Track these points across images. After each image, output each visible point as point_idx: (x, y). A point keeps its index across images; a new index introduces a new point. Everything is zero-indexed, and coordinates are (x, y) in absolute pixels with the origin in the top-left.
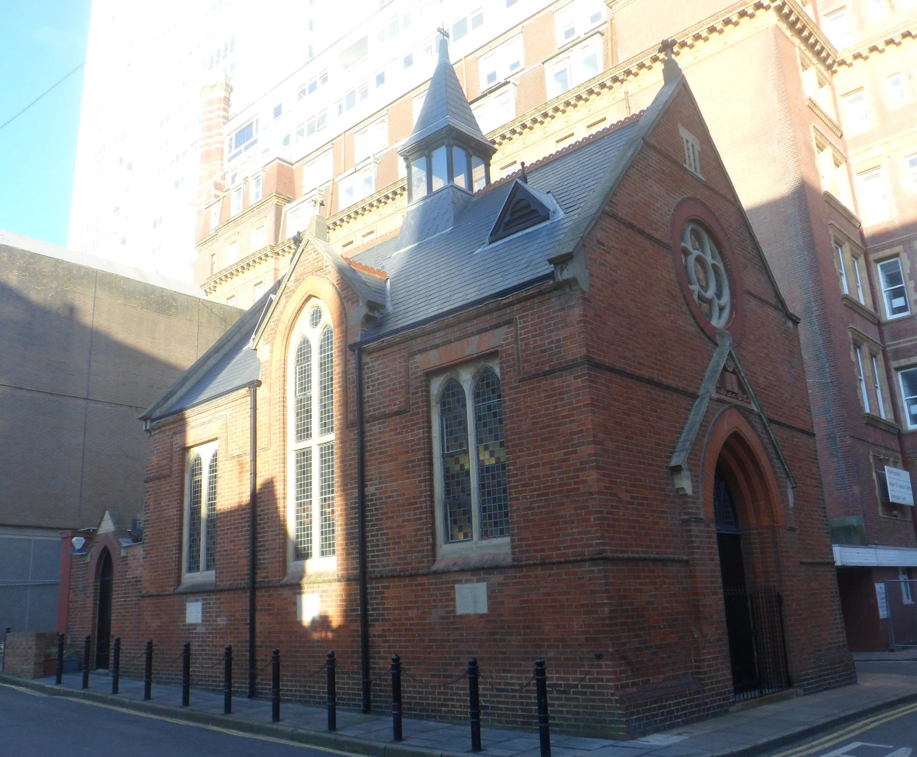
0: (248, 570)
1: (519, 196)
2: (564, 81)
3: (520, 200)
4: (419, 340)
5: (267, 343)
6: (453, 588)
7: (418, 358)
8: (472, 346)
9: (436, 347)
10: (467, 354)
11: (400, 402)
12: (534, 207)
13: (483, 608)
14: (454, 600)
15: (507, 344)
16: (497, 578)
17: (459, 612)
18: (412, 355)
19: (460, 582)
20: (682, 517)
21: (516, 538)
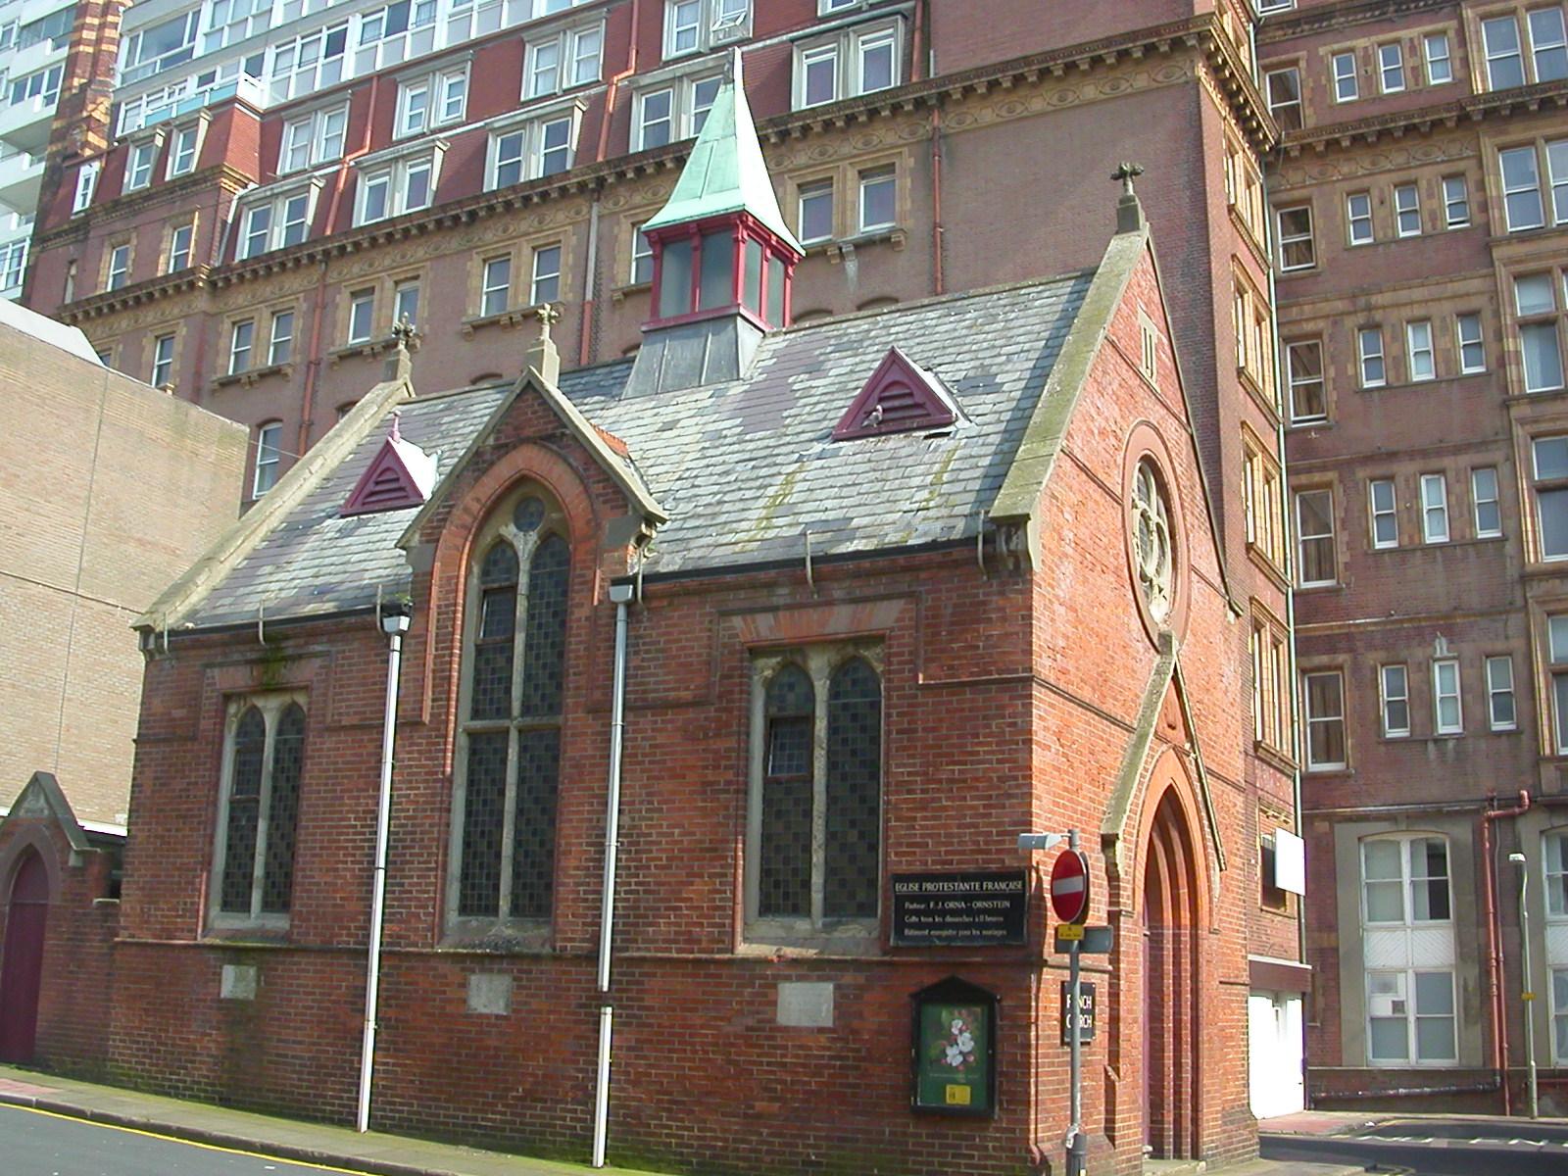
0: (558, 892)
1: (387, 462)
2: (503, 304)
3: (388, 469)
4: (742, 594)
5: (428, 542)
6: (775, 986)
7: (737, 622)
8: (840, 620)
9: (774, 609)
10: (827, 630)
11: (697, 688)
12: (402, 483)
13: (825, 1017)
14: (774, 1003)
15: (901, 629)
16: (849, 978)
17: (827, 1020)
18: (726, 614)
19: (788, 978)
20: (1251, 957)
21: (621, 921)
